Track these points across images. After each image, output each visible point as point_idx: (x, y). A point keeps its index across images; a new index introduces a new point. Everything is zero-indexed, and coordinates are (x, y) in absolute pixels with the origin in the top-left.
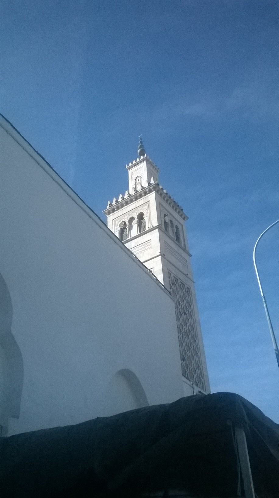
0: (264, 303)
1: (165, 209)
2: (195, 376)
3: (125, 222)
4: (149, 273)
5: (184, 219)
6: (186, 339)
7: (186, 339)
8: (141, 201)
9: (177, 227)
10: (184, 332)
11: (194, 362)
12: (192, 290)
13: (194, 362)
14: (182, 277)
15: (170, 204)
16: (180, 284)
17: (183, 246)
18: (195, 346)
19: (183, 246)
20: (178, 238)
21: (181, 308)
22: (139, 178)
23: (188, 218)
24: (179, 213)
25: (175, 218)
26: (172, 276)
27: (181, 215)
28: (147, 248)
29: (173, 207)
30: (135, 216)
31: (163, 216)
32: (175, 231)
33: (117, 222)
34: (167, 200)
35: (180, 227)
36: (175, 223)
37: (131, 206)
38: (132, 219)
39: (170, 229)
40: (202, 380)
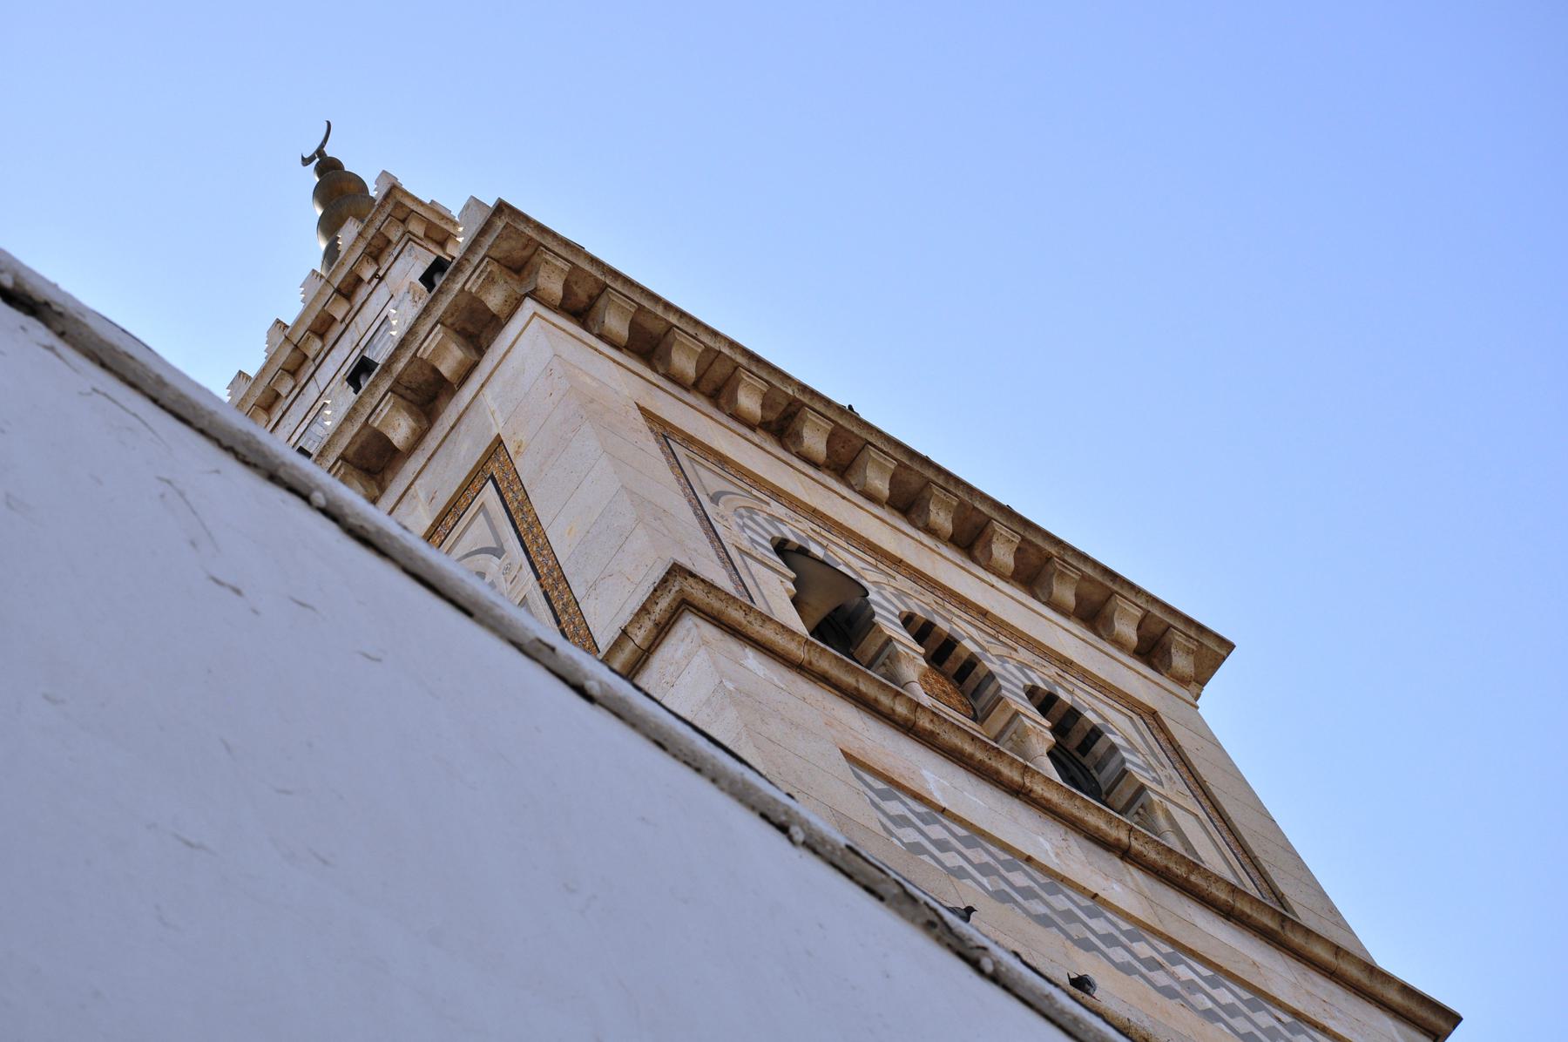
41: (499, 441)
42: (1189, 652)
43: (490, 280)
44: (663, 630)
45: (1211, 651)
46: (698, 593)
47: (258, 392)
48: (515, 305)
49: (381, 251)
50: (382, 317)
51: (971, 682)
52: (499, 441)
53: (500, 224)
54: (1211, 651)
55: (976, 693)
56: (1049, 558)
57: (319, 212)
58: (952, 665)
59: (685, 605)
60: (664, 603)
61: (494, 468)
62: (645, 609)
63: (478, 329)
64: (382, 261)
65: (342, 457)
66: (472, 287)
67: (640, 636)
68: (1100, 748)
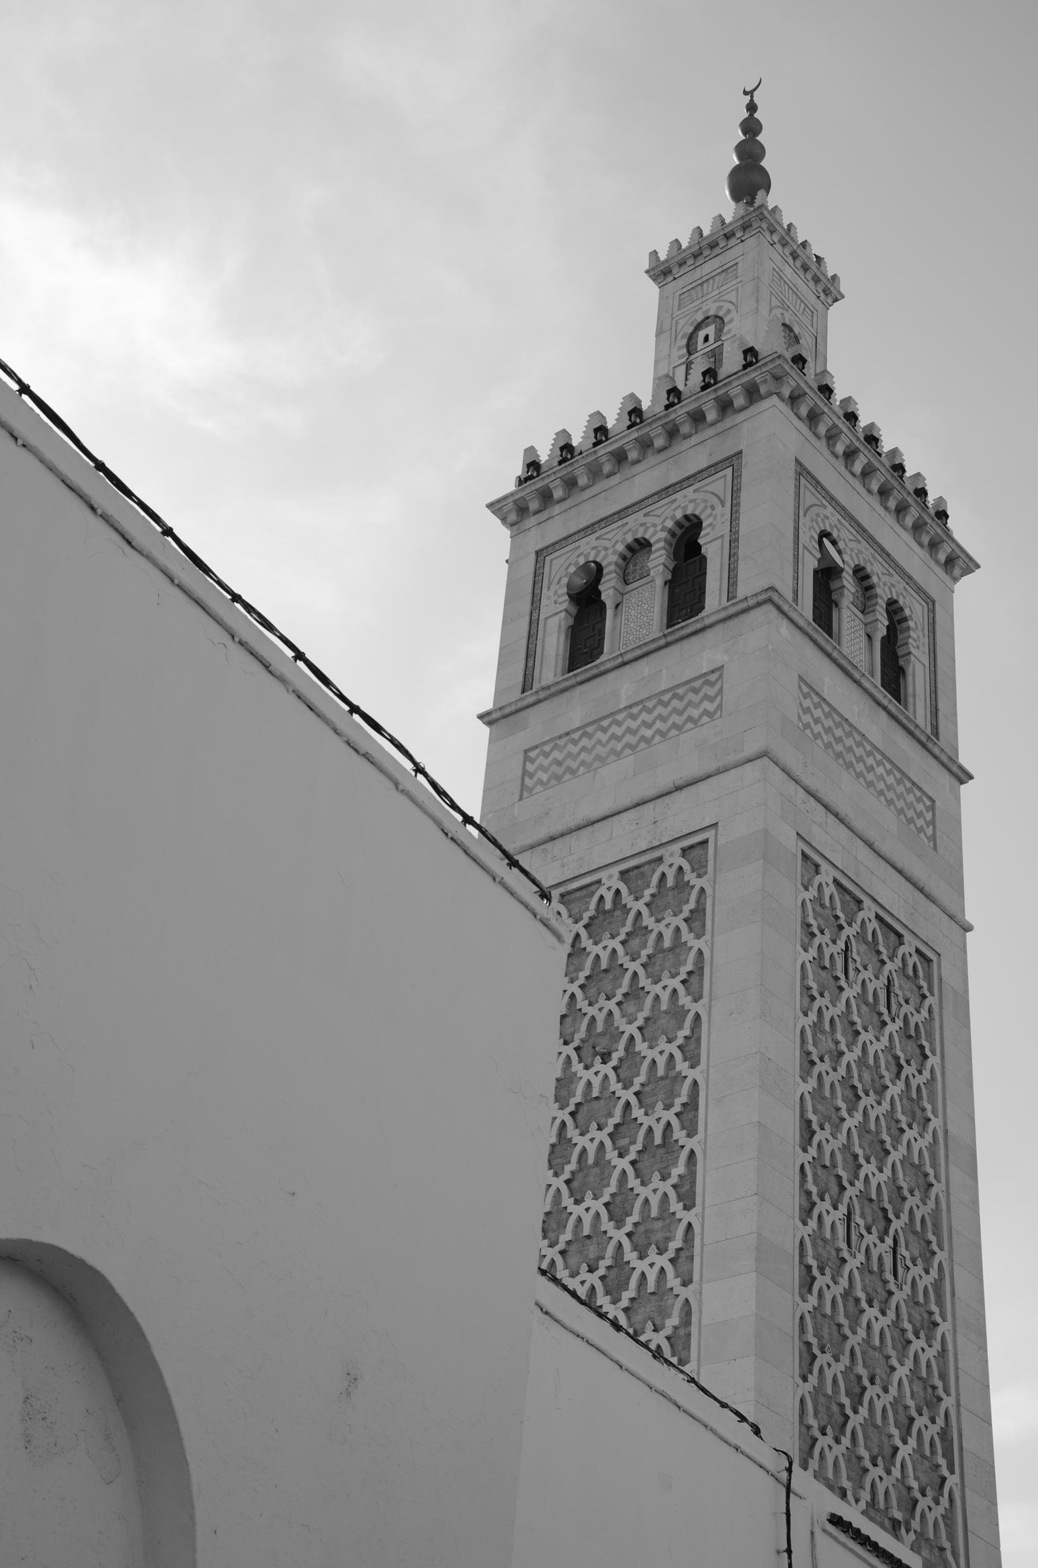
1: (832, 499)
2: (905, 1451)
3: (600, 568)
4: (414, 787)
5: (949, 563)
6: (871, 1239)
7: (871, 1239)
8: (695, 454)
9: (893, 608)
11: (902, 1372)
13: (902, 1372)
14: (890, 894)
15: (867, 473)
17: (921, 716)
18: (928, 1280)
20: (894, 676)
21: (862, 1062)
22: (710, 330)
24: (918, 528)
26: (827, 875)
27: (933, 546)
28: (695, 713)
29: (884, 493)
30: (658, 538)
31: (808, 537)
32: (882, 631)
33: (557, 564)
34: (850, 455)
35: (914, 609)
36: (886, 586)
37: (646, 478)
38: (640, 546)
39: (847, 616)
40: (952, 1481)
41: (741, 452)
42: (962, 568)
43: (765, 381)
44: (759, 604)
45: (971, 566)
46: (776, 598)
47: (680, 258)
48: (770, 394)
49: (748, 227)
50: (656, 854)
51: (869, 593)
52: (741, 452)
53: (778, 362)
54: (971, 566)
55: (869, 598)
56: (926, 524)
57: (737, 162)
58: (865, 584)
59: (770, 600)
60: (764, 597)
61: (735, 463)
62: (756, 595)
63: (753, 394)
64: (747, 231)
65: (688, 413)
66: (758, 380)
67: (751, 602)
68: (904, 625)
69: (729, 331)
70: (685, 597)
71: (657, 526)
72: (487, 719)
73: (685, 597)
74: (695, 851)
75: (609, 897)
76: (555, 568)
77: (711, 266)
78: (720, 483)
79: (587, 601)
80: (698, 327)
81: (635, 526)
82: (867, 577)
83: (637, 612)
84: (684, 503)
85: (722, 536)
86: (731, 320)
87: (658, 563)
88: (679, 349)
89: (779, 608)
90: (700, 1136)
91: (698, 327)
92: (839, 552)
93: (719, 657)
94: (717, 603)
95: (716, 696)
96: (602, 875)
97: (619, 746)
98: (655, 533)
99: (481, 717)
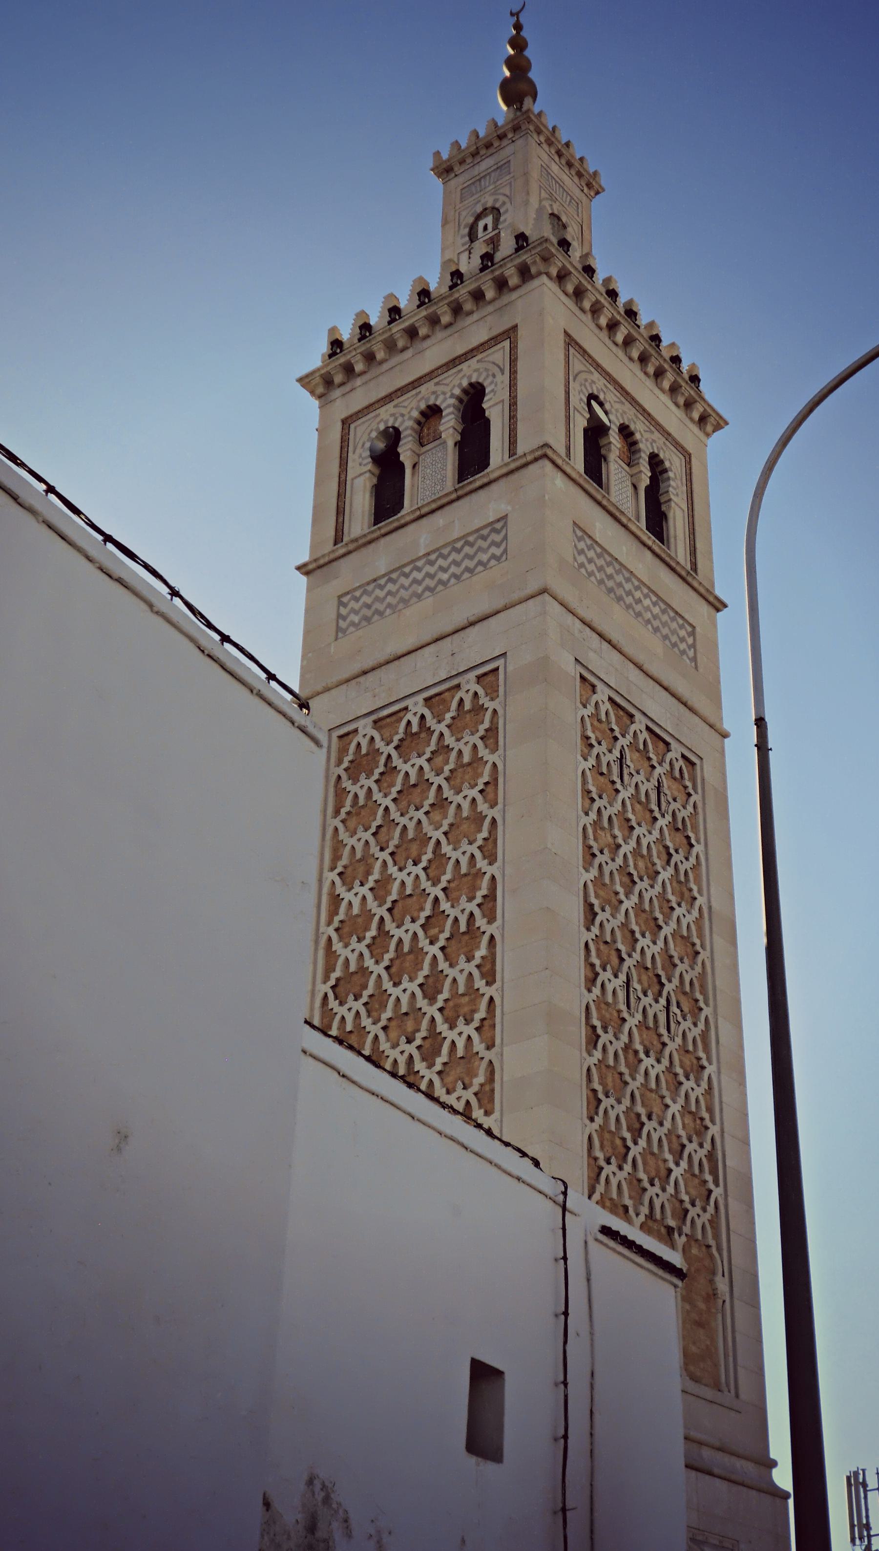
0: (856, 1523)
9: (655, 461)
10: (641, 966)
12: (707, 770)
14: (657, 707)
16: (606, 706)
17: (681, 554)
19: (681, 554)
20: (657, 520)
21: (637, 852)
22: (489, 220)
23: (569, 141)
25: (644, 412)
31: (578, 400)
32: (645, 481)
34: (612, 326)
35: (673, 462)
36: (648, 442)
37: (436, 351)
38: (433, 412)
39: (615, 468)
69: (505, 220)
70: (473, 455)
71: (447, 394)
72: (304, 570)
73: (473, 455)
74: (488, 678)
75: (415, 722)
76: (359, 434)
77: (486, 164)
78: (500, 354)
79: (388, 465)
80: (478, 217)
81: (427, 394)
82: (632, 434)
83: (430, 471)
84: (469, 373)
85: (503, 401)
86: (507, 211)
87: (449, 426)
88: (463, 237)
89: (553, 462)
90: (498, 922)
91: (478, 217)
92: (606, 413)
93: (503, 508)
94: (500, 459)
95: (502, 541)
96: (409, 702)
97: (420, 589)
98: (445, 399)
99: (298, 568)
